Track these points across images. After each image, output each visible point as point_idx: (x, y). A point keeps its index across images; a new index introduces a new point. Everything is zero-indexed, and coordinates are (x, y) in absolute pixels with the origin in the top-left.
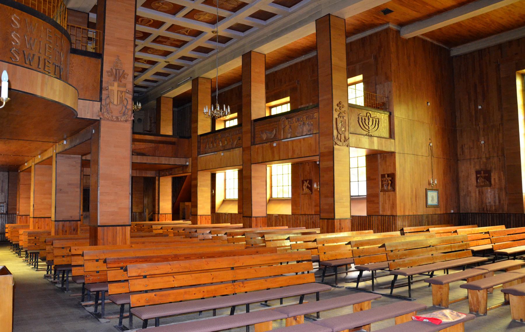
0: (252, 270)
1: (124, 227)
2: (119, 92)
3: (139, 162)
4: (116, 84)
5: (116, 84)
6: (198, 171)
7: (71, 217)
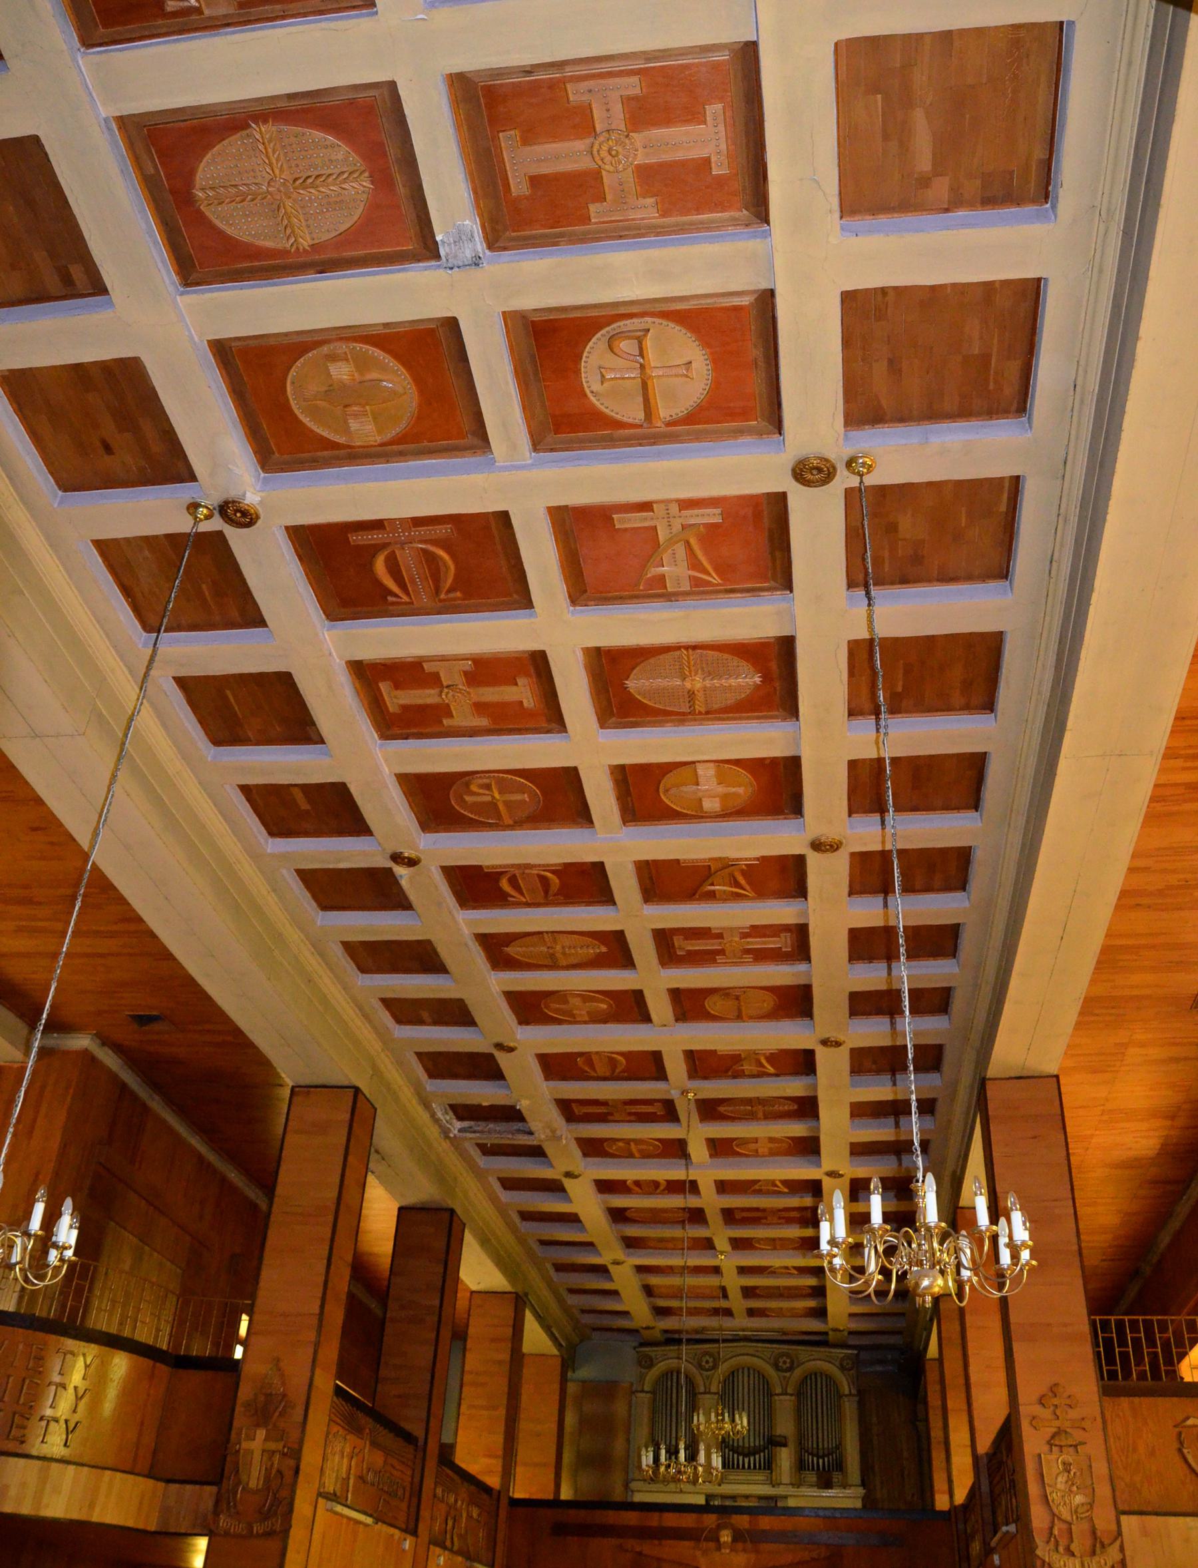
4: (261, 1434)
5: (261, 1434)
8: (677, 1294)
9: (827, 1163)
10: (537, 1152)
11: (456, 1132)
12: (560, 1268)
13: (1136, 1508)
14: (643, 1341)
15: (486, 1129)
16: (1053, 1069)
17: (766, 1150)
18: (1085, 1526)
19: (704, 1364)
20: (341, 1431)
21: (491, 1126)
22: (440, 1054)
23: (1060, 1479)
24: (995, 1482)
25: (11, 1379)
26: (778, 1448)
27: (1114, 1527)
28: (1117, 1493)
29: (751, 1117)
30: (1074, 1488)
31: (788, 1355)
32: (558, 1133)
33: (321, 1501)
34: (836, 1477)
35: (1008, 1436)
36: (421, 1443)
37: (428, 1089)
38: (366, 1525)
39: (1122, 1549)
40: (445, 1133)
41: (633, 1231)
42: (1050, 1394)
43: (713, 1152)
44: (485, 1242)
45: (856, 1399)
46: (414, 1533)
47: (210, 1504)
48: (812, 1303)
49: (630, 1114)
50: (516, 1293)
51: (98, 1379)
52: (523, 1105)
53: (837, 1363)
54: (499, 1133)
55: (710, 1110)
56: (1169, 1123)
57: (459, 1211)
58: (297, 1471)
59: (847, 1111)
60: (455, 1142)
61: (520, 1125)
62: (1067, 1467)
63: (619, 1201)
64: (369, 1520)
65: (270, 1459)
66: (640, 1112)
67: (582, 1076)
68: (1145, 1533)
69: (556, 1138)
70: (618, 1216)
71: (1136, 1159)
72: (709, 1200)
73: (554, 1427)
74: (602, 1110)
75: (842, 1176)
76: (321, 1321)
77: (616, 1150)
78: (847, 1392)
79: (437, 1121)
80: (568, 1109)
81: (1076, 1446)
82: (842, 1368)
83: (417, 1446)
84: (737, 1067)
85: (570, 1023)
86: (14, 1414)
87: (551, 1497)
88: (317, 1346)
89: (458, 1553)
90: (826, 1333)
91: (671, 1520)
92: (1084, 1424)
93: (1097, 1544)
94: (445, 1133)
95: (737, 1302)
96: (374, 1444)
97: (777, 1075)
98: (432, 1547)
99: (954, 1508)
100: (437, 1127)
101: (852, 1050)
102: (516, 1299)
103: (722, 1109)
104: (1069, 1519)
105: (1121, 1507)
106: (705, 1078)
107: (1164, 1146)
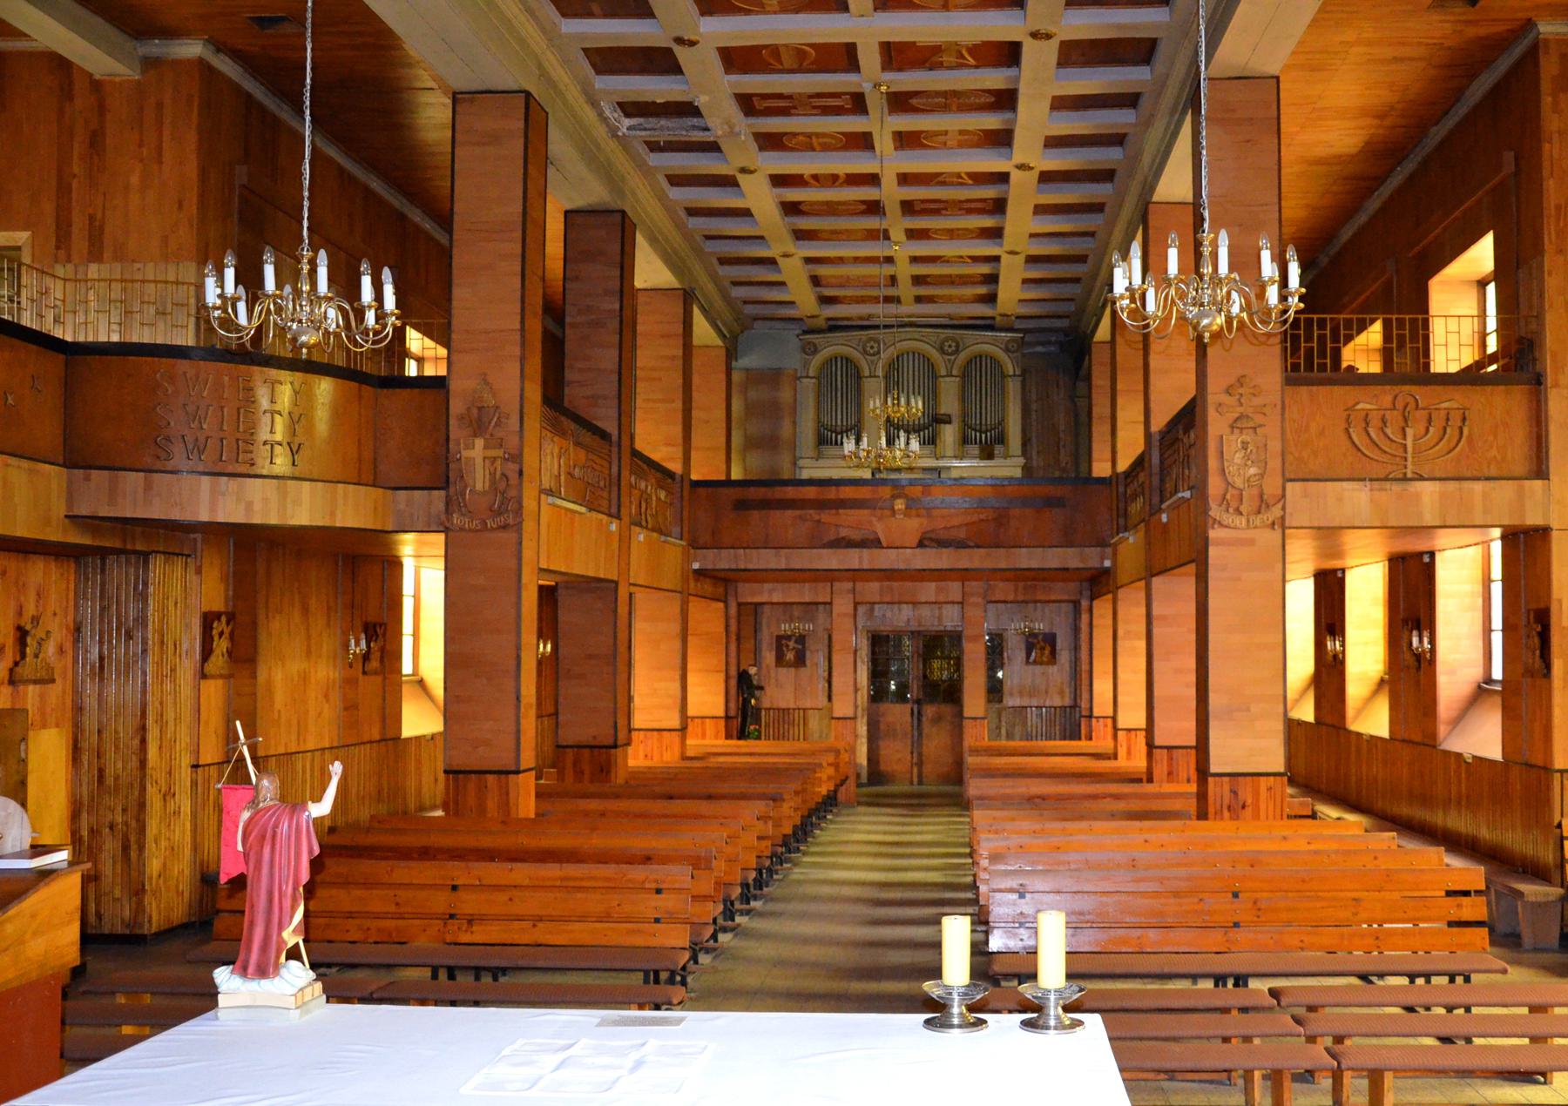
0: (502, 897)
1: (503, 776)
2: (487, 461)
3: (945, 567)
4: (479, 443)
5: (479, 443)
6: (1117, 588)
7: (594, 737)
8: (844, 283)
9: (1019, 156)
10: (713, 147)
11: (625, 130)
12: (724, 261)
13: (1301, 477)
14: (810, 328)
15: (659, 125)
16: (1274, 69)
17: (955, 143)
18: (1255, 491)
19: (868, 349)
20: (549, 434)
21: (663, 122)
22: (611, 49)
23: (1237, 455)
24: (1166, 456)
25: (225, 410)
26: (942, 425)
27: (1280, 492)
28: (1287, 465)
29: (944, 108)
30: (1249, 462)
31: (953, 339)
32: (737, 129)
33: (543, 497)
34: (998, 449)
35: (1189, 417)
36: (615, 438)
37: (597, 87)
38: (581, 513)
39: (1284, 508)
40: (613, 132)
41: (805, 223)
42: (1237, 384)
43: (898, 144)
44: (653, 240)
45: (1020, 379)
46: (618, 517)
47: (441, 506)
48: (982, 290)
49: (814, 107)
50: (684, 290)
51: (303, 398)
52: (702, 101)
53: (1003, 346)
54: (668, 128)
55: (900, 102)
56: (1376, 122)
57: (630, 213)
58: (521, 473)
59: (1047, 104)
60: (623, 142)
61: (695, 121)
62: (1245, 445)
63: (793, 195)
64: (583, 510)
65: (493, 463)
66: (825, 104)
67: (765, 68)
68: (1305, 495)
69: (733, 134)
70: (791, 209)
71: (1335, 157)
72: (890, 193)
73: (722, 414)
74: (782, 104)
75: (1031, 168)
76: (523, 337)
77: (795, 144)
78: (1011, 373)
79: (605, 120)
80: (747, 103)
81: (1255, 428)
82: (1007, 350)
83: (611, 441)
84: (936, 59)
85: (757, 13)
86: (238, 440)
87: (723, 478)
88: (523, 359)
89: (653, 530)
90: (993, 318)
91: (847, 492)
92: (1265, 410)
93: (1262, 504)
94: (613, 132)
95: (906, 290)
96: (577, 444)
97: (976, 67)
98: (632, 527)
99: (1115, 475)
100: (604, 126)
101: (1063, 43)
102: (685, 295)
103: (914, 101)
104: (1241, 486)
105: (1287, 475)
106: (900, 70)
107: (1368, 143)
